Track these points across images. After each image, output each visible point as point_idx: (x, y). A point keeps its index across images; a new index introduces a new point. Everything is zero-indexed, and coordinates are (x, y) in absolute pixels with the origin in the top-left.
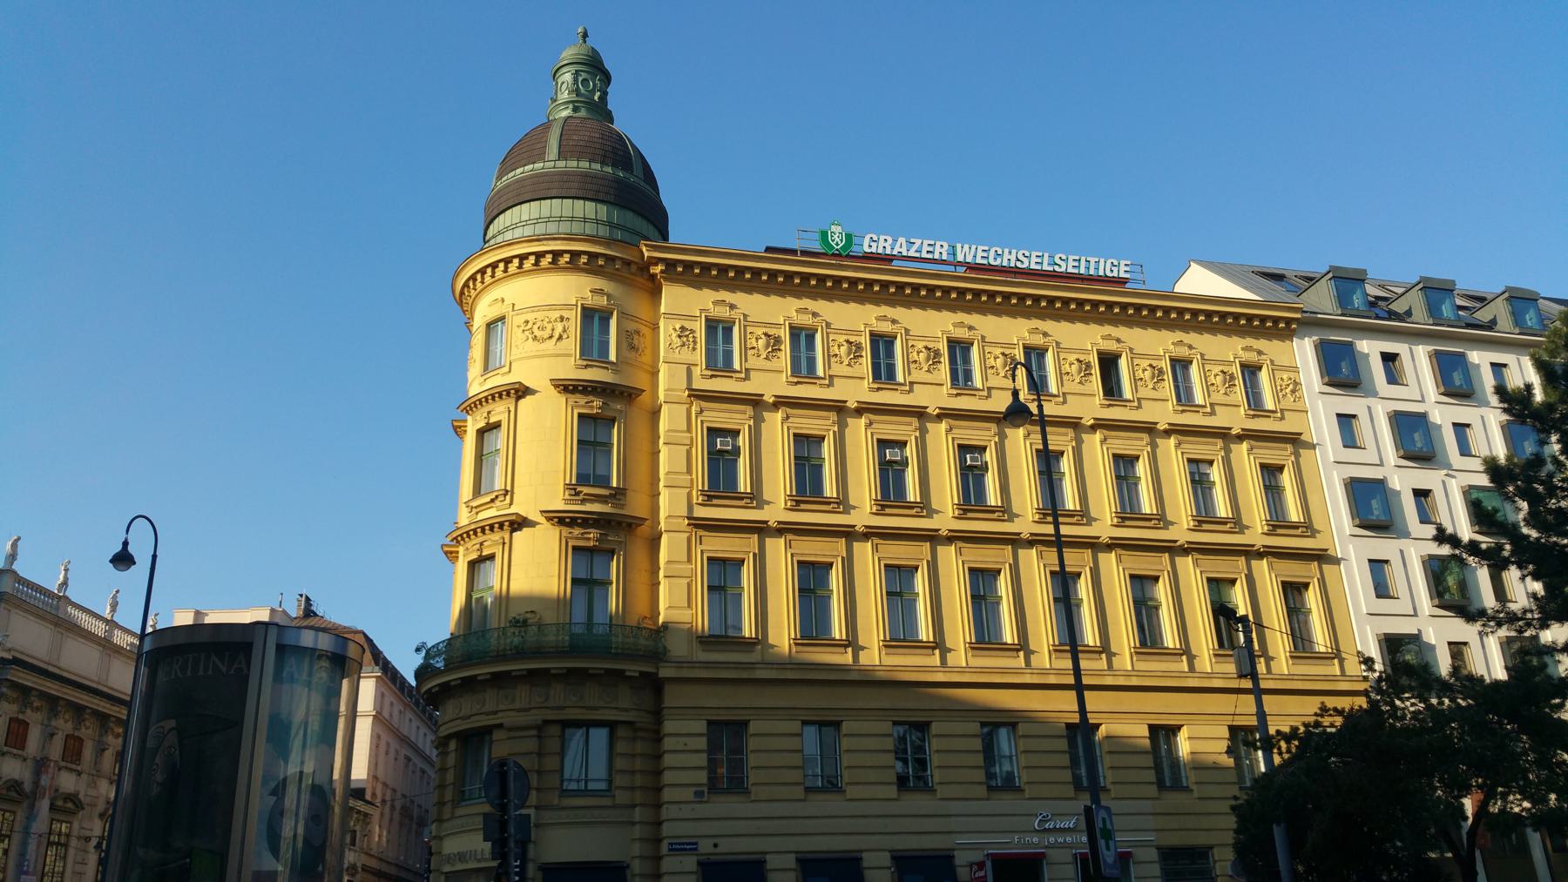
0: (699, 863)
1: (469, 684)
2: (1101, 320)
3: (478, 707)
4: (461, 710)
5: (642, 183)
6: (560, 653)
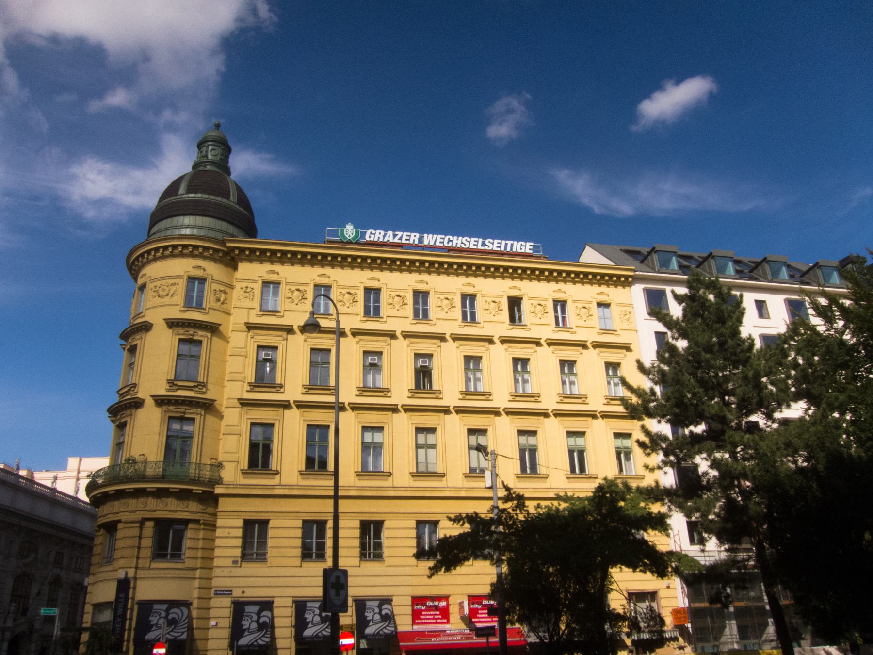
0: (233, 602)
1: (120, 495)
2: (192, 255)
3: (111, 509)
4: (113, 508)
5: (237, 207)
6: (155, 479)
